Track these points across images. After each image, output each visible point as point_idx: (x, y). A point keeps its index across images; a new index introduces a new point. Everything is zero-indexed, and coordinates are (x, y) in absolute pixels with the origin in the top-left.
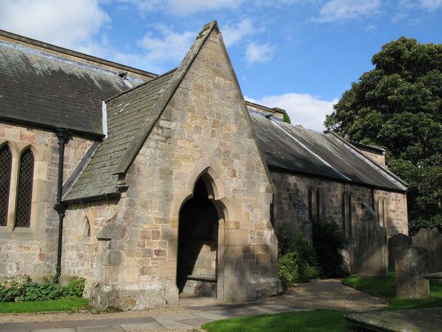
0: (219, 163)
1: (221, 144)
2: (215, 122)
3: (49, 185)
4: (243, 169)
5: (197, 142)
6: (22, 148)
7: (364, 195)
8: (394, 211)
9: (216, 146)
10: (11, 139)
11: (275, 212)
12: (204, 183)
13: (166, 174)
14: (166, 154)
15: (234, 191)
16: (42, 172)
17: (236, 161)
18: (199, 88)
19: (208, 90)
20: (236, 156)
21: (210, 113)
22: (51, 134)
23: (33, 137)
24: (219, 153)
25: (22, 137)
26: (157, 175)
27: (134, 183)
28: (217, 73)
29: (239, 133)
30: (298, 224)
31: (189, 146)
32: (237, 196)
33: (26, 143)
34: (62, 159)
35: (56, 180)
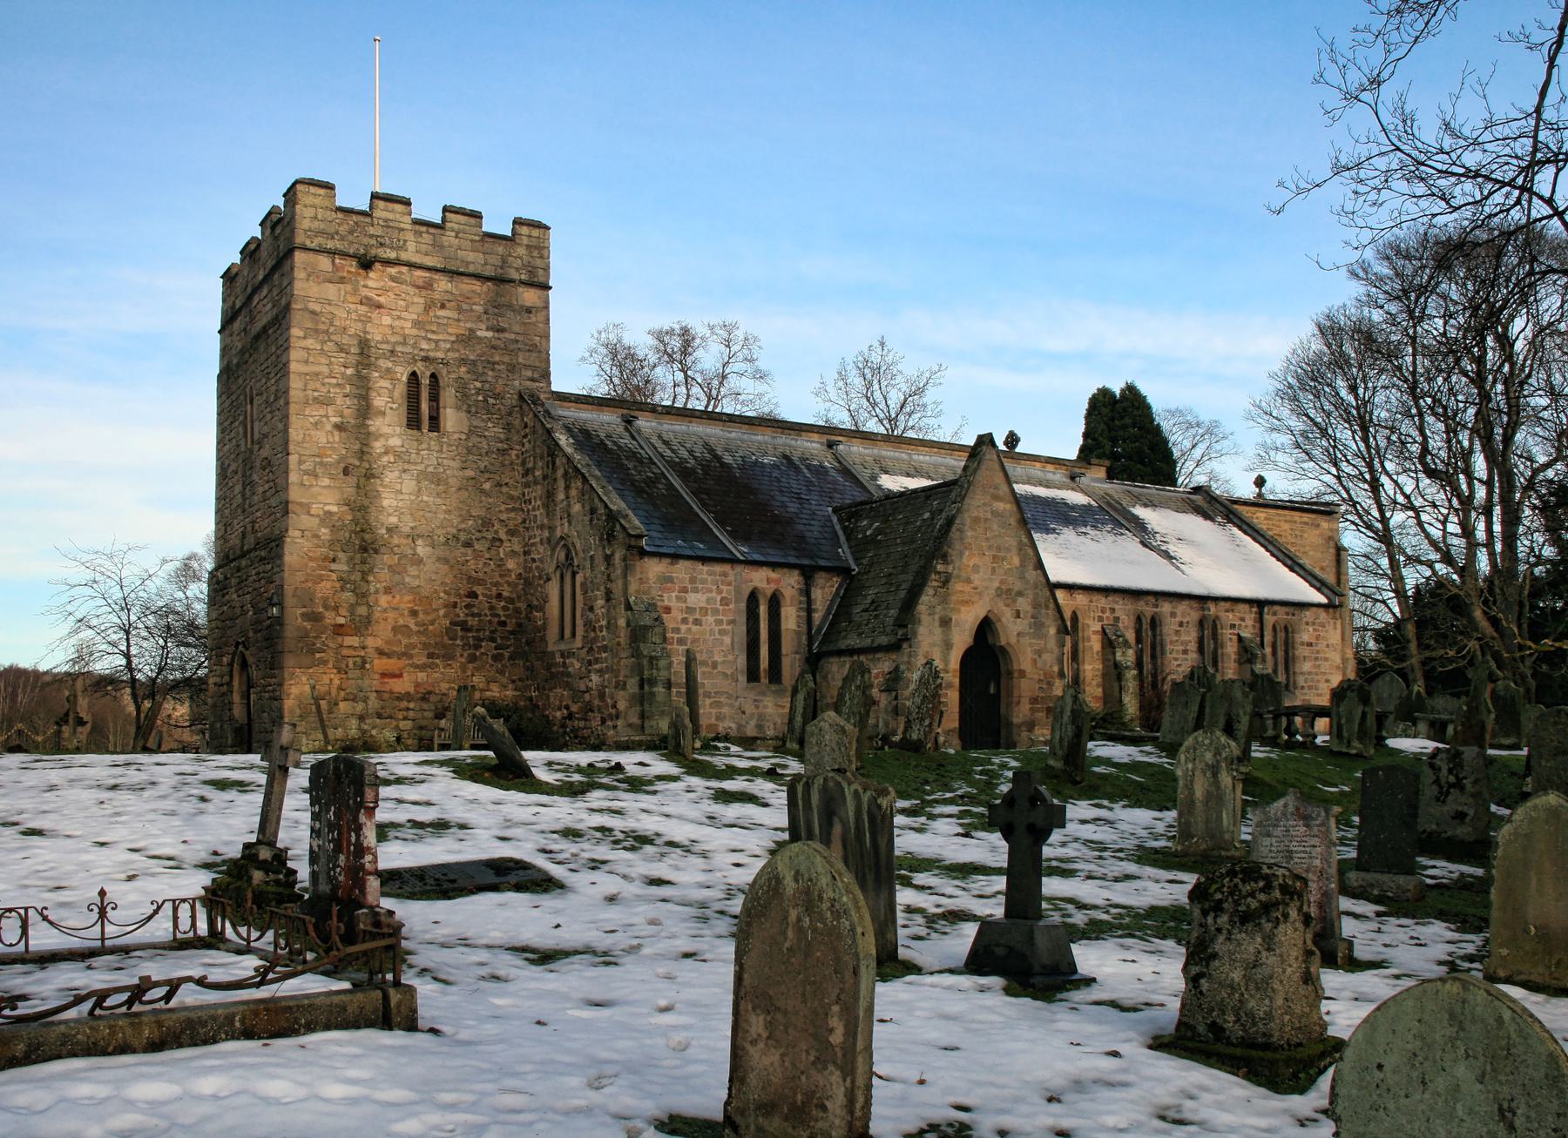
0: (1001, 605)
1: (1002, 582)
2: (994, 557)
3: (798, 633)
4: (1029, 608)
5: (976, 583)
6: (769, 593)
7: (1243, 619)
8: (1310, 644)
9: (996, 584)
10: (758, 585)
11: (1030, 552)
12: (986, 628)
13: (945, 623)
14: (944, 600)
15: (1019, 634)
16: (791, 618)
17: (1020, 600)
18: (976, 520)
19: (986, 520)
20: (1020, 594)
21: (990, 548)
22: (796, 572)
23: (778, 581)
24: (1000, 593)
25: (769, 581)
26: (937, 623)
27: (915, 634)
28: (996, 498)
29: (1023, 565)
30: (20, 725)
31: (967, 588)
32: (1022, 640)
33: (773, 587)
34: (809, 602)
35: (804, 628)
